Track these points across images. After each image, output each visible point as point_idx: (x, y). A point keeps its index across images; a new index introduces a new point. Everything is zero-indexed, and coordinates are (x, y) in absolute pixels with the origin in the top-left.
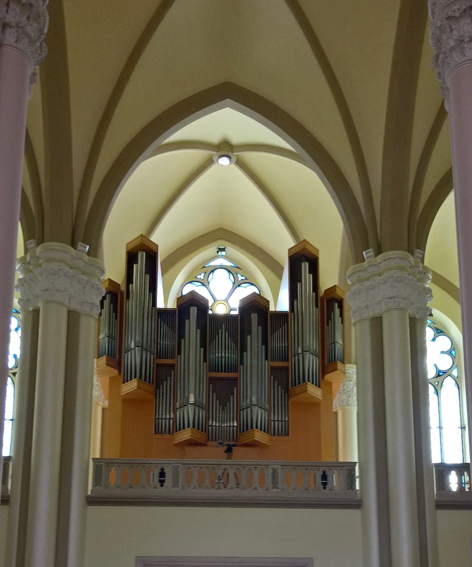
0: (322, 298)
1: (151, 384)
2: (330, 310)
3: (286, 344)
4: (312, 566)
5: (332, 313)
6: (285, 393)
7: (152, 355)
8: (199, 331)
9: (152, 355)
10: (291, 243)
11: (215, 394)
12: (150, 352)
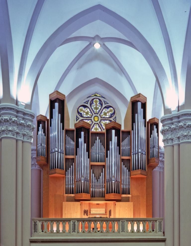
0: (148, 123)
1: (113, 193)
2: (152, 129)
3: (129, 148)
4: (190, 125)
5: (153, 131)
6: (128, 171)
7: (63, 154)
8: (60, 115)
9: (63, 154)
10: (133, 95)
11: (93, 174)
12: (62, 153)
